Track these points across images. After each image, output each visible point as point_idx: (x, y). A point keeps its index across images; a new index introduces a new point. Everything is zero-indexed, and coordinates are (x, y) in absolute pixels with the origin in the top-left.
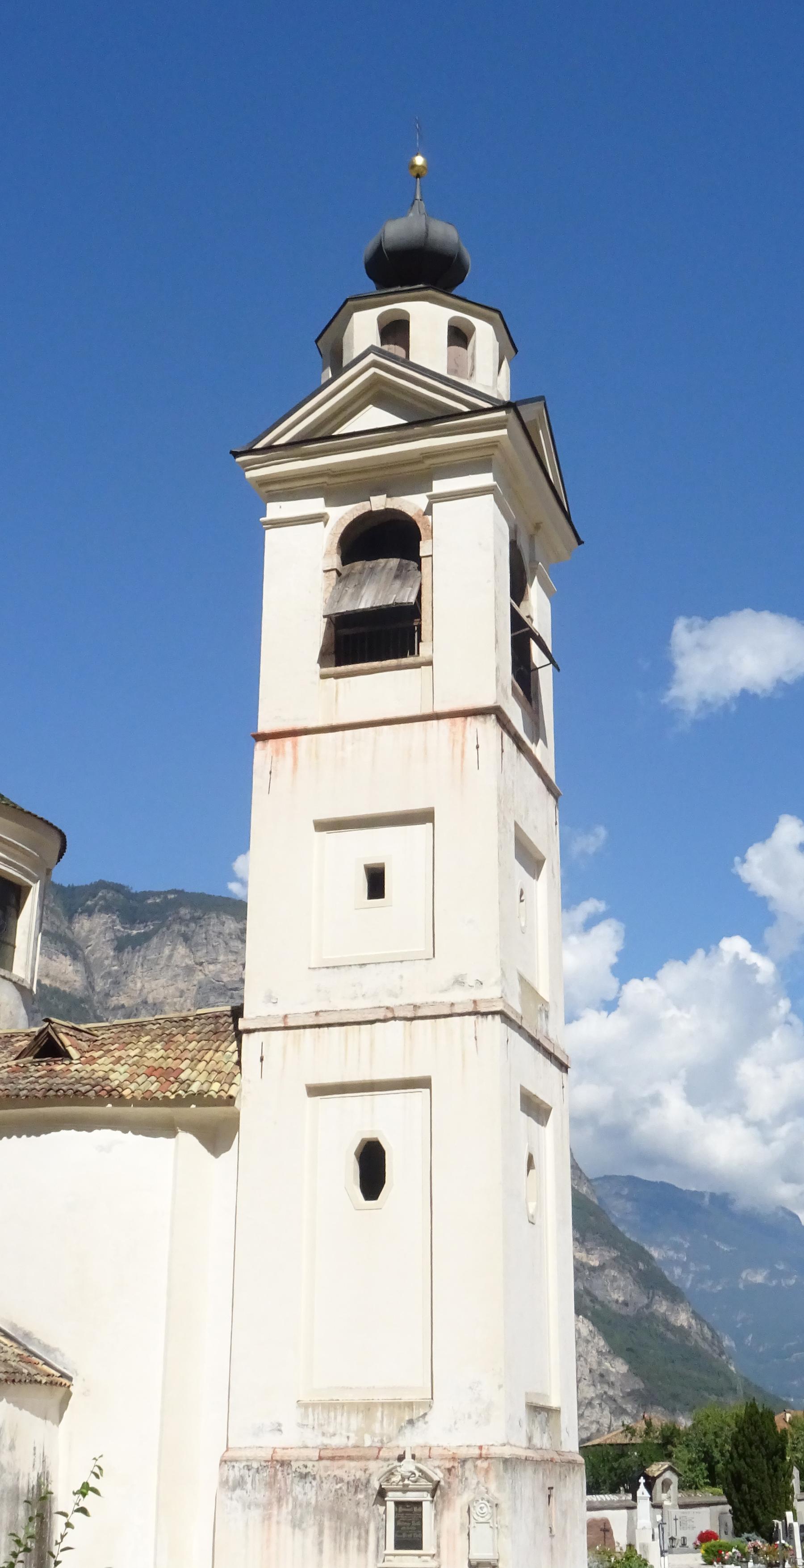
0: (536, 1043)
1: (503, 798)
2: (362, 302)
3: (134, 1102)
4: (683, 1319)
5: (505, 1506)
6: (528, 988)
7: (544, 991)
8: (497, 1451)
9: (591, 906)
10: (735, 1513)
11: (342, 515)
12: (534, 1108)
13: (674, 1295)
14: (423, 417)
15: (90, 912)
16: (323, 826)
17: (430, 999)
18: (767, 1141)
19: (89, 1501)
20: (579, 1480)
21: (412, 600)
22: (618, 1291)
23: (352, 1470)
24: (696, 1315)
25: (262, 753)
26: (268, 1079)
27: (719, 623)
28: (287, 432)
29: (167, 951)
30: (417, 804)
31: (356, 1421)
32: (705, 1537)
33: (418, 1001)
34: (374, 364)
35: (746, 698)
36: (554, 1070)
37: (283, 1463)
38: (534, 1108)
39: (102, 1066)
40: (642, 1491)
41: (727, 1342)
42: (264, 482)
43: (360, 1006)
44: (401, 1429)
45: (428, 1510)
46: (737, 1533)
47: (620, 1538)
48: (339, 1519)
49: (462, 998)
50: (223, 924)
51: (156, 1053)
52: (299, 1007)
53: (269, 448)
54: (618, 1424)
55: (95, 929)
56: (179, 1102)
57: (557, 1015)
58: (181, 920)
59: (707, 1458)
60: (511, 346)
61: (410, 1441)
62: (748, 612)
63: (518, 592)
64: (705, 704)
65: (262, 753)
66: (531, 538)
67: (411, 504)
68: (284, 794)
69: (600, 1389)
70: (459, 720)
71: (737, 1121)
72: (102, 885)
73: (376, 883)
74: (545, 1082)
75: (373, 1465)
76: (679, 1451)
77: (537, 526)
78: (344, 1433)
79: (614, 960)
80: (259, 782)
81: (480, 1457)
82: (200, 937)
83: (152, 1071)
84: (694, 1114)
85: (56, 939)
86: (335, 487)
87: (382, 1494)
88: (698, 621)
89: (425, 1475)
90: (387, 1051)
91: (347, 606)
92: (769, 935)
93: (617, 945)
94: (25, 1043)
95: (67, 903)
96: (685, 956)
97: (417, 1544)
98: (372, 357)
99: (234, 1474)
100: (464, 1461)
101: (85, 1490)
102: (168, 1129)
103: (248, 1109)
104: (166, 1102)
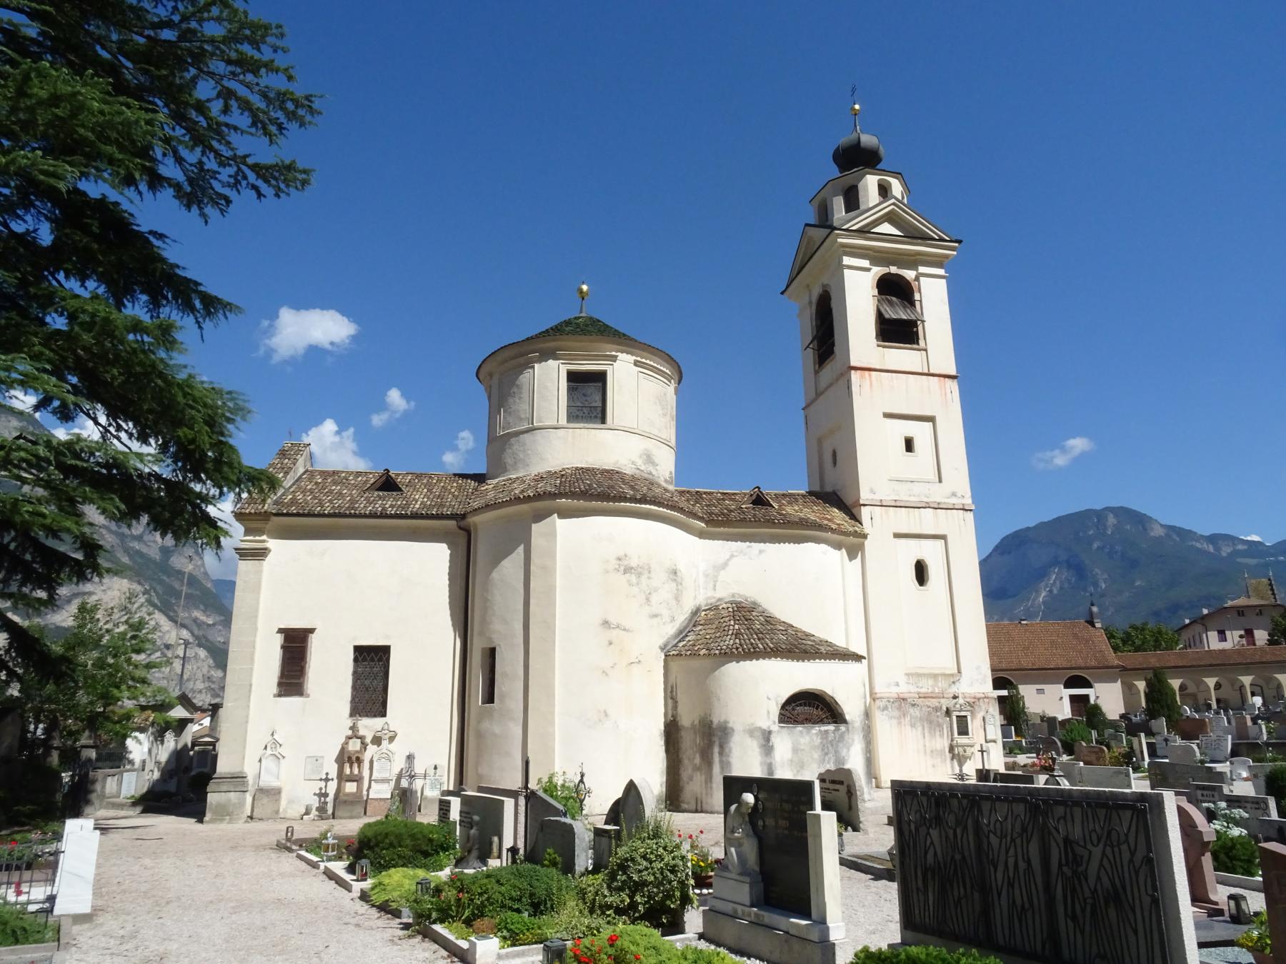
11: (878, 271)
23: (934, 703)
31: (931, 682)
43: (913, 500)
48: (929, 722)
52: (887, 494)
53: (846, 230)
61: (954, 690)
62: (318, 311)
67: (909, 274)
69: (207, 684)
78: (927, 686)
80: (855, 389)
86: (877, 257)
90: (927, 521)
97: (967, 733)
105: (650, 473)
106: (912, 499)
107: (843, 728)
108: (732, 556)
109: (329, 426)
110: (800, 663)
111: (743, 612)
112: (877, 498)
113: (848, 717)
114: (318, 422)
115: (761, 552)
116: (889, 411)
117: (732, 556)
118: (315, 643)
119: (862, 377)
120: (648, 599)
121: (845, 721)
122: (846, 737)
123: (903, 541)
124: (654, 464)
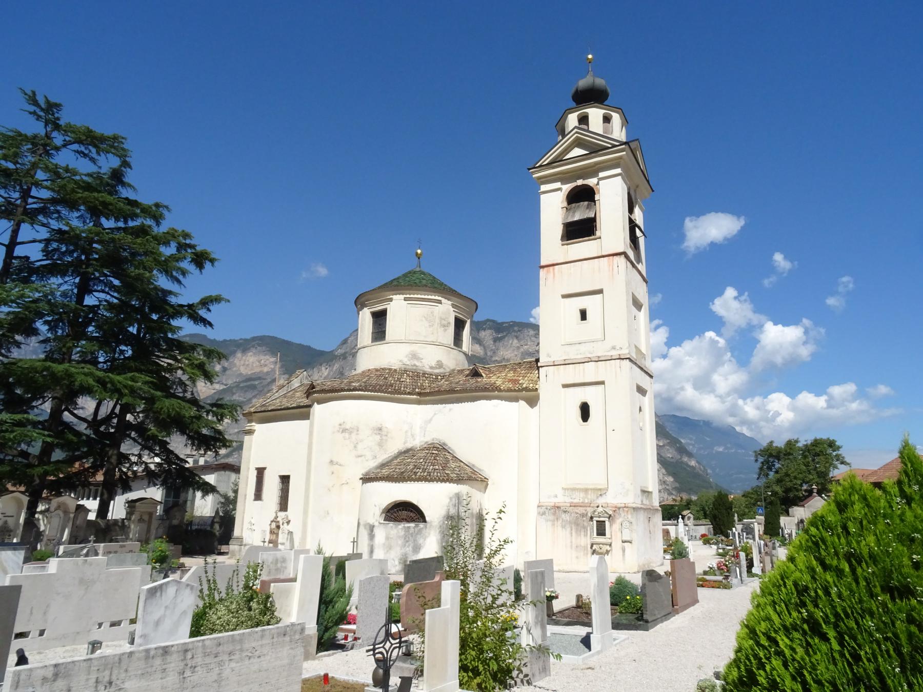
0: (641, 369)
1: (628, 283)
2: (571, 110)
3: (504, 391)
4: (693, 463)
5: (634, 523)
6: (638, 350)
7: (644, 351)
8: (630, 505)
9: (657, 322)
10: (714, 528)
11: (567, 188)
12: (641, 391)
13: (690, 455)
14: (595, 150)
15: (485, 330)
16: (564, 296)
18: (723, 402)
19: (502, 515)
20: (659, 516)
22: (670, 454)
23: (581, 510)
24: (698, 462)
25: (542, 272)
26: (549, 382)
27: (702, 218)
28: (546, 160)
30: (597, 288)
31: (582, 495)
32: (703, 536)
34: (577, 133)
35: (713, 245)
36: (648, 378)
38: (641, 391)
39: (493, 379)
40: (680, 520)
41: (709, 471)
42: (539, 178)
43: (579, 357)
46: (715, 535)
47: (673, 535)
48: (577, 525)
49: (615, 353)
51: (511, 374)
52: (558, 357)
53: (541, 166)
54: (670, 498)
55: (487, 335)
56: (519, 390)
57: (648, 359)
58: (514, 331)
59: (703, 509)
60: (626, 121)
61: (601, 501)
62: (713, 213)
63: (631, 210)
64: (697, 248)
65: (542, 272)
66: (635, 191)
67: (592, 182)
68: (551, 286)
71: (712, 396)
72: (488, 320)
73: (583, 315)
74: (645, 382)
75: (588, 509)
76: (692, 507)
77: (637, 187)
78: (578, 498)
79: (665, 340)
80: (542, 282)
82: (522, 336)
83: (510, 381)
84: (696, 393)
85: (476, 340)
86: (564, 178)
87: (592, 518)
88: (694, 218)
89: (606, 512)
90: (589, 372)
91: (570, 220)
92: (723, 330)
93: (666, 335)
94: (468, 372)
95: (477, 327)
96: (691, 338)
97: (604, 535)
99: (542, 510)
101: (501, 512)
102: (516, 400)
103: (542, 392)
104: (515, 391)
105: (415, 365)
106: (579, 357)
107: (422, 525)
109: (730, 292)
110: (397, 484)
112: (550, 360)
113: (427, 519)
114: (721, 293)
115: (450, 410)
118: (266, 472)
119: (548, 272)
120: (355, 447)
121: (425, 521)
122: (424, 531)
123: (571, 389)
124: (418, 359)
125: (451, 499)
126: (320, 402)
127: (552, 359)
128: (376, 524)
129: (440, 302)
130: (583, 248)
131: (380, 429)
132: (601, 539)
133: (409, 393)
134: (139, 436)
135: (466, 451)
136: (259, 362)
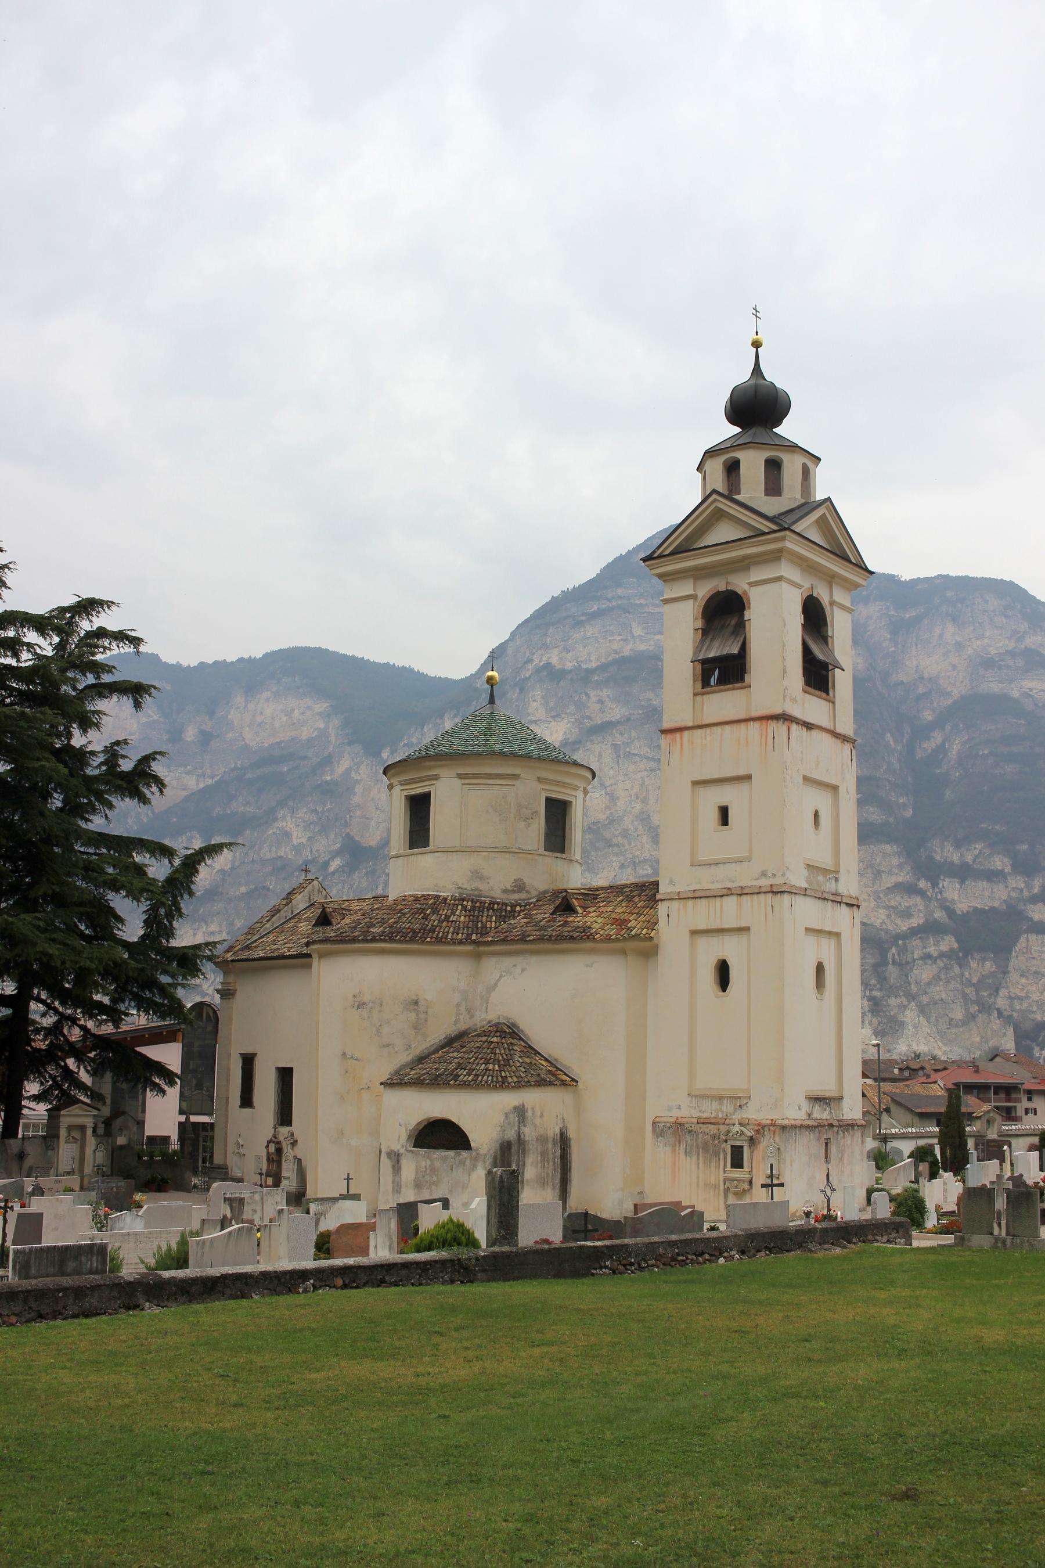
8: (779, 1122)
11: (705, 590)
17: (750, 883)
21: (735, 650)
23: (713, 1129)
29: (937, 631)
30: (743, 772)
31: (715, 1105)
33: (743, 884)
34: (715, 500)
37: (681, 1125)
44: (735, 1110)
45: (746, 1149)
48: (708, 1149)
50: (987, 602)
52: (683, 886)
53: (660, 557)
67: (739, 583)
70: (764, 722)
78: (710, 1110)
81: (771, 1125)
90: (729, 913)
98: (714, 496)
100: (764, 1127)
105: (477, 889)
107: (465, 1154)
108: (501, 976)
111: (508, 1033)
113: (472, 1144)
116: (699, 777)
117: (501, 976)
120: (378, 1031)
124: (482, 878)
125: (507, 1115)
126: (322, 955)
127: (676, 889)
128: (402, 1151)
129: (516, 777)
130: (725, 703)
131: (416, 1003)
132: (737, 1174)
133: (461, 942)
134: (52, 994)
135: (547, 1036)
136: (289, 714)
